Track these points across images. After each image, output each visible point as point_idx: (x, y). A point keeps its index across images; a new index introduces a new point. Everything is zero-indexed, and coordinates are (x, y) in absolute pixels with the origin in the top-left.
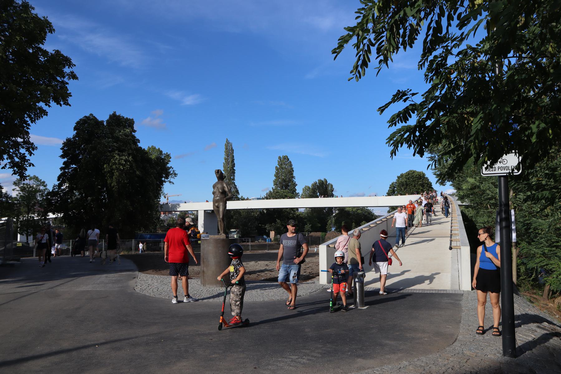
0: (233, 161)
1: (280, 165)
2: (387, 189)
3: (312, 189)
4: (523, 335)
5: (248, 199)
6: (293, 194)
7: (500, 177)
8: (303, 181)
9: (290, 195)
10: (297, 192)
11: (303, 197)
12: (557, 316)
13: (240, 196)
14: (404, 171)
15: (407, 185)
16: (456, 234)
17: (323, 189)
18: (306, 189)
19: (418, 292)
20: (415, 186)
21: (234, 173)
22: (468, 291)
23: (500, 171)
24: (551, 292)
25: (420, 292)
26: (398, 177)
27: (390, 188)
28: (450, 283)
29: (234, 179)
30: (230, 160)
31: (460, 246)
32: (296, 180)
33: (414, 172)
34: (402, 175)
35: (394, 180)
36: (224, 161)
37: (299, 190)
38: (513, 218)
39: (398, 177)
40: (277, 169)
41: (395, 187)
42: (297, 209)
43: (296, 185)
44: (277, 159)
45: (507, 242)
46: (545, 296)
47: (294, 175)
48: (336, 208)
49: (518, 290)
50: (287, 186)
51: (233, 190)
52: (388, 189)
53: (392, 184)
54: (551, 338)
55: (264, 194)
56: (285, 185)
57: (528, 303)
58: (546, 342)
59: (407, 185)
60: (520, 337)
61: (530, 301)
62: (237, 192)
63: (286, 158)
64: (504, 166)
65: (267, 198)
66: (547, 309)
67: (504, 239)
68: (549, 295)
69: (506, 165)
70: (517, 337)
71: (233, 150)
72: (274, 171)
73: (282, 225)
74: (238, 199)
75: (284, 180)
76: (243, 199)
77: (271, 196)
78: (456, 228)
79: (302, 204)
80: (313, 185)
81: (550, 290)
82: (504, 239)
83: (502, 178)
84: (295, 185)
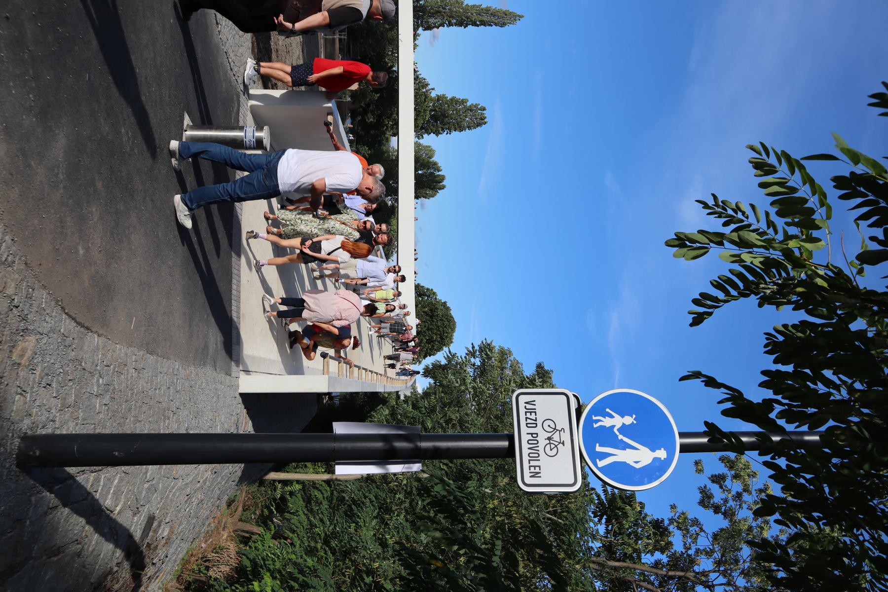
0: (483, 23)
1: (473, 109)
2: (426, 284)
3: (429, 162)
4: (118, 487)
5: (415, 46)
6: (421, 128)
7: (511, 438)
8: (444, 147)
9: (421, 122)
10: (425, 136)
11: (417, 145)
12: (203, 545)
13: (420, 31)
14: (453, 313)
15: (432, 317)
16: (352, 373)
17: (428, 182)
18: (430, 152)
19: (234, 287)
20: (428, 329)
21: (460, 24)
22: (238, 387)
23: (525, 438)
24: (247, 535)
25: (234, 292)
26: (445, 303)
27: (428, 289)
28: (256, 354)
29: (450, 24)
30: (485, 18)
31: (328, 373)
32: (444, 136)
33: (453, 330)
34: (448, 309)
35: (441, 297)
36: (484, 6)
37: (429, 140)
38: (395, 469)
39: (445, 303)
40: (464, 101)
41: (428, 296)
42: (396, 134)
43: (437, 135)
44: (482, 104)
45: (334, 450)
46: (240, 525)
47: (455, 134)
48: (397, 200)
49: (254, 482)
50: (435, 118)
51: (432, 20)
52: (426, 286)
53: (434, 293)
54: (117, 546)
55: (423, 74)
56: (438, 116)
57: (226, 498)
58: (102, 534)
59: (432, 317)
60: (110, 480)
61: (230, 504)
62: (428, 28)
63: (480, 122)
64: (541, 448)
65: (416, 78)
66: (217, 528)
67: (343, 445)
68: (243, 531)
69: (541, 452)
70: (111, 471)
71: (503, 25)
72: (460, 96)
73: (368, 105)
74: (415, 29)
75: (444, 116)
76: (415, 36)
77: (420, 84)
78: (364, 377)
79: (405, 142)
80: (435, 164)
81: (253, 533)
82: (343, 445)
83: (506, 444)
84: (437, 133)
